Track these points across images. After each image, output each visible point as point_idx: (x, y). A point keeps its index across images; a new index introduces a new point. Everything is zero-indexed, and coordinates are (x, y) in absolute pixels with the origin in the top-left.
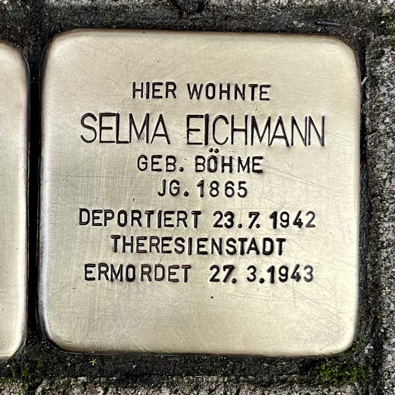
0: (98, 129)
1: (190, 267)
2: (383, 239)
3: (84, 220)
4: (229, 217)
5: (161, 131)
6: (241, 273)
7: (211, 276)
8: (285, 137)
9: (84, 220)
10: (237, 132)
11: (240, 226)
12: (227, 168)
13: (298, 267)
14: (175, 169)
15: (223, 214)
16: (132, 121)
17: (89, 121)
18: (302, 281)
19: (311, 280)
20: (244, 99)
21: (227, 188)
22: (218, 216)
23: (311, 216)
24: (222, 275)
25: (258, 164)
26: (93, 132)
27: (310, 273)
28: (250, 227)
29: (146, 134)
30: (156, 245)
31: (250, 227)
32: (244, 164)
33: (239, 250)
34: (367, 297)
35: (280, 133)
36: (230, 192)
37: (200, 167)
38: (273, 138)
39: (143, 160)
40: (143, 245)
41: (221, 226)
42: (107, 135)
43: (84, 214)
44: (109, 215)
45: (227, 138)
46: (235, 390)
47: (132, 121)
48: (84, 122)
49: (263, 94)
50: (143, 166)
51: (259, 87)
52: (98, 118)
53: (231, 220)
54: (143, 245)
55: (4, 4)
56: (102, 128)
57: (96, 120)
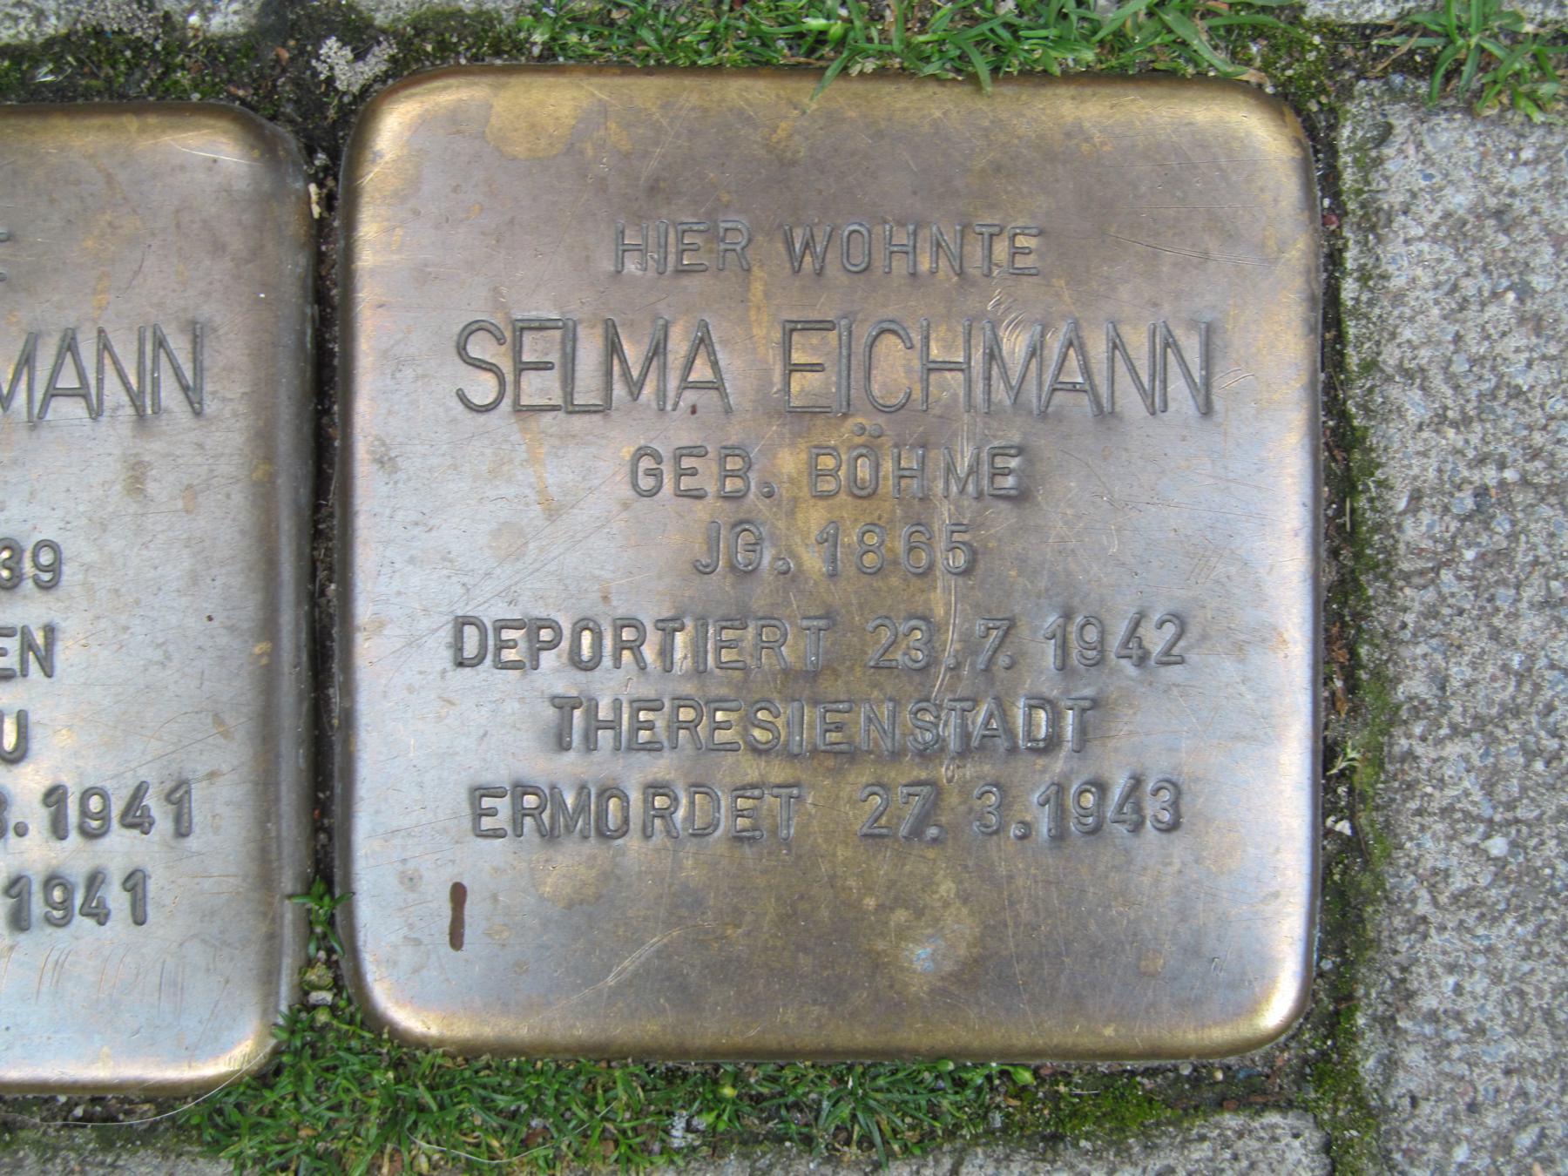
0: (507, 367)
2: (1401, 692)
3: (470, 649)
9: (470, 649)
10: (532, 374)
17: (479, 348)
19: (1174, 826)
27: (1175, 805)
34: (1328, 680)
35: (68, 380)
39: (647, 463)
40: (492, 812)
42: (539, 388)
43: (471, 633)
44: (546, 635)
46: (947, 1163)
47: (613, 348)
48: (469, 348)
49: (1018, 257)
50: (646, 483)
52: (508, 334)
54: (492, 812)
55: (327, 37)
56: (521, 368)
57: (500, 340)
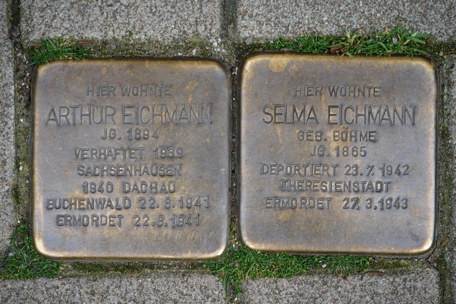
1: (337, 166)
4: (369, 201)
5: (312, 115)
6: (363, 203)
7: (345, 172)
8: (390, 120)
9: (265, 171)
11: (375, 208)
12: (353, 139)
13: (398, 199)
14: (321, 139)
15: (351, 166)
16: (294, 110)
18: (400, 208)
19: (406, 207)
20: (364, 96)
21: (353, 151)
22: (348, 168)
23: (405, 168)
24: (351, 204)
25: (373, 136)
26: (347, 120)
28: (368, 175)
29: (378, 119)
30: (310, 186)
31: (368, 175)
32: (364, 135)
33: (361, 188)
36: (355, 153)
37: (337, 139)
38: (275, 116)
41: (349, 174)
45: (353, 120)
51: (373, 88)
53: (370, 203)
56: (276, 114)
